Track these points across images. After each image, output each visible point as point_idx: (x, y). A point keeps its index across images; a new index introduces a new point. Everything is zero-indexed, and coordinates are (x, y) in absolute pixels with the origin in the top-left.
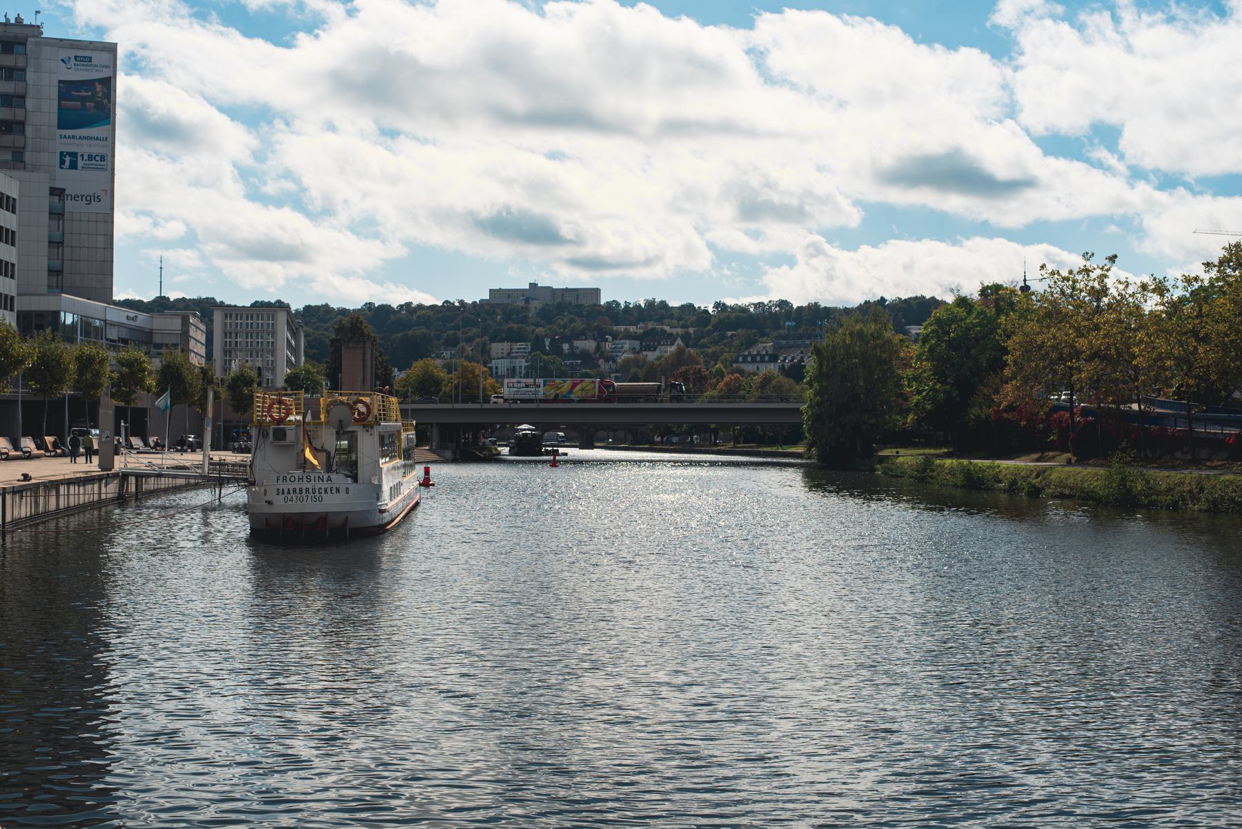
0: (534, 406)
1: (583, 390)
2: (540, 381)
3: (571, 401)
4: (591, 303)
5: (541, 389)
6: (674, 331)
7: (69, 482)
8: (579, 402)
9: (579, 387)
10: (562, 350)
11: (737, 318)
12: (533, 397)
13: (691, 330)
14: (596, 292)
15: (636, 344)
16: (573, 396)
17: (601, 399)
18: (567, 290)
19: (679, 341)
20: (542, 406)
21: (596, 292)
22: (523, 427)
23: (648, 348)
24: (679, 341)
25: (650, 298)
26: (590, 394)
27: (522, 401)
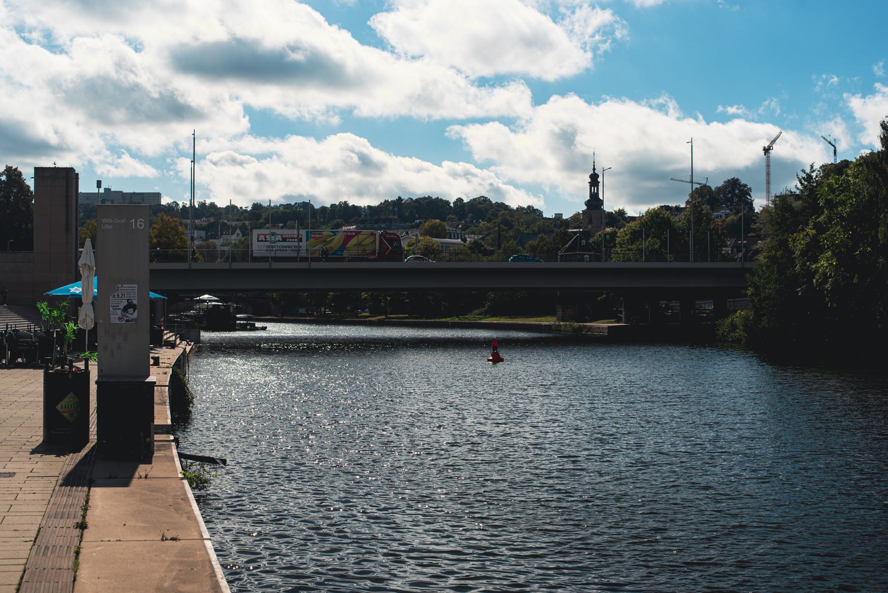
0: (304, 265)
1: (359, 244)
2: (303, 232)
3: (342, 259)
4: (156, 203)
5: (303, 244)
6: (234, 223)
7: (87, 36)
8: (354, 260)
9: (354, 241)
10: (716, 109)
11: (283, 213)
12: (295, 254)
13: (247, 223)
14: (158, 196)
15: (203, 233)
16: (345, 254)
17: (381, 257)
18: (134, 194)
19: (238, 231)
20: (315, 265)
21: (158, 196)
22: (206, 297)
23: (214, 237)
24: (238, 231)
25: (202, 200)
26: (369, 249)
27: (276, 259)
